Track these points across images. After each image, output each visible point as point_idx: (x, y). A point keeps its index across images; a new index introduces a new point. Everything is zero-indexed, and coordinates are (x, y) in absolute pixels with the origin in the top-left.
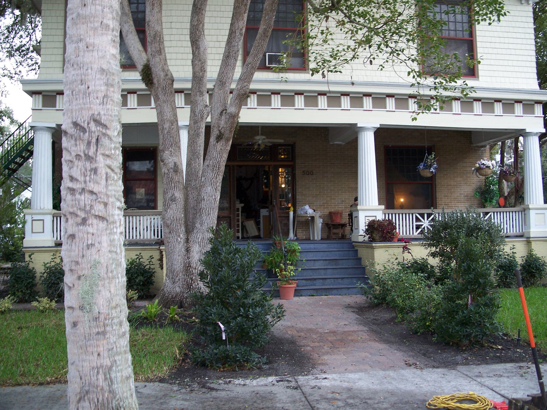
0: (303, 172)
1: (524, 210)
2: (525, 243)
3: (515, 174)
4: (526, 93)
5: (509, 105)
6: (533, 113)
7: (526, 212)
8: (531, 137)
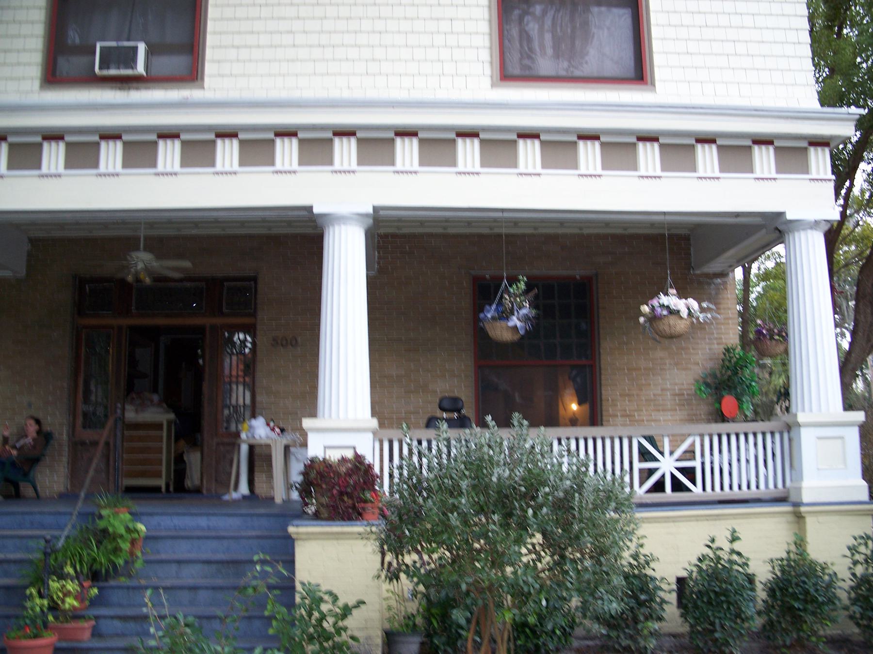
0: (275, 339)
1: (789, 428)
2: (791, 518)
3: (768, 331)
4: (787, 118)
5: (736, 151)
6: (806, 170)
7: (792, 434)
8: (803, 234)
